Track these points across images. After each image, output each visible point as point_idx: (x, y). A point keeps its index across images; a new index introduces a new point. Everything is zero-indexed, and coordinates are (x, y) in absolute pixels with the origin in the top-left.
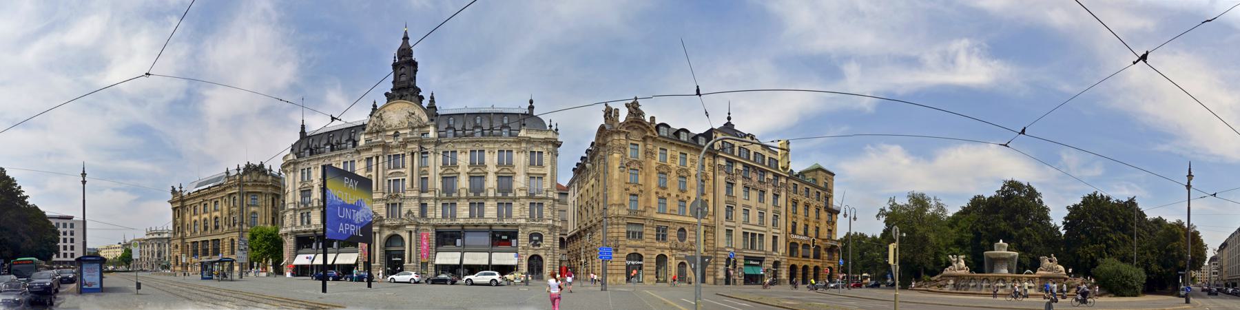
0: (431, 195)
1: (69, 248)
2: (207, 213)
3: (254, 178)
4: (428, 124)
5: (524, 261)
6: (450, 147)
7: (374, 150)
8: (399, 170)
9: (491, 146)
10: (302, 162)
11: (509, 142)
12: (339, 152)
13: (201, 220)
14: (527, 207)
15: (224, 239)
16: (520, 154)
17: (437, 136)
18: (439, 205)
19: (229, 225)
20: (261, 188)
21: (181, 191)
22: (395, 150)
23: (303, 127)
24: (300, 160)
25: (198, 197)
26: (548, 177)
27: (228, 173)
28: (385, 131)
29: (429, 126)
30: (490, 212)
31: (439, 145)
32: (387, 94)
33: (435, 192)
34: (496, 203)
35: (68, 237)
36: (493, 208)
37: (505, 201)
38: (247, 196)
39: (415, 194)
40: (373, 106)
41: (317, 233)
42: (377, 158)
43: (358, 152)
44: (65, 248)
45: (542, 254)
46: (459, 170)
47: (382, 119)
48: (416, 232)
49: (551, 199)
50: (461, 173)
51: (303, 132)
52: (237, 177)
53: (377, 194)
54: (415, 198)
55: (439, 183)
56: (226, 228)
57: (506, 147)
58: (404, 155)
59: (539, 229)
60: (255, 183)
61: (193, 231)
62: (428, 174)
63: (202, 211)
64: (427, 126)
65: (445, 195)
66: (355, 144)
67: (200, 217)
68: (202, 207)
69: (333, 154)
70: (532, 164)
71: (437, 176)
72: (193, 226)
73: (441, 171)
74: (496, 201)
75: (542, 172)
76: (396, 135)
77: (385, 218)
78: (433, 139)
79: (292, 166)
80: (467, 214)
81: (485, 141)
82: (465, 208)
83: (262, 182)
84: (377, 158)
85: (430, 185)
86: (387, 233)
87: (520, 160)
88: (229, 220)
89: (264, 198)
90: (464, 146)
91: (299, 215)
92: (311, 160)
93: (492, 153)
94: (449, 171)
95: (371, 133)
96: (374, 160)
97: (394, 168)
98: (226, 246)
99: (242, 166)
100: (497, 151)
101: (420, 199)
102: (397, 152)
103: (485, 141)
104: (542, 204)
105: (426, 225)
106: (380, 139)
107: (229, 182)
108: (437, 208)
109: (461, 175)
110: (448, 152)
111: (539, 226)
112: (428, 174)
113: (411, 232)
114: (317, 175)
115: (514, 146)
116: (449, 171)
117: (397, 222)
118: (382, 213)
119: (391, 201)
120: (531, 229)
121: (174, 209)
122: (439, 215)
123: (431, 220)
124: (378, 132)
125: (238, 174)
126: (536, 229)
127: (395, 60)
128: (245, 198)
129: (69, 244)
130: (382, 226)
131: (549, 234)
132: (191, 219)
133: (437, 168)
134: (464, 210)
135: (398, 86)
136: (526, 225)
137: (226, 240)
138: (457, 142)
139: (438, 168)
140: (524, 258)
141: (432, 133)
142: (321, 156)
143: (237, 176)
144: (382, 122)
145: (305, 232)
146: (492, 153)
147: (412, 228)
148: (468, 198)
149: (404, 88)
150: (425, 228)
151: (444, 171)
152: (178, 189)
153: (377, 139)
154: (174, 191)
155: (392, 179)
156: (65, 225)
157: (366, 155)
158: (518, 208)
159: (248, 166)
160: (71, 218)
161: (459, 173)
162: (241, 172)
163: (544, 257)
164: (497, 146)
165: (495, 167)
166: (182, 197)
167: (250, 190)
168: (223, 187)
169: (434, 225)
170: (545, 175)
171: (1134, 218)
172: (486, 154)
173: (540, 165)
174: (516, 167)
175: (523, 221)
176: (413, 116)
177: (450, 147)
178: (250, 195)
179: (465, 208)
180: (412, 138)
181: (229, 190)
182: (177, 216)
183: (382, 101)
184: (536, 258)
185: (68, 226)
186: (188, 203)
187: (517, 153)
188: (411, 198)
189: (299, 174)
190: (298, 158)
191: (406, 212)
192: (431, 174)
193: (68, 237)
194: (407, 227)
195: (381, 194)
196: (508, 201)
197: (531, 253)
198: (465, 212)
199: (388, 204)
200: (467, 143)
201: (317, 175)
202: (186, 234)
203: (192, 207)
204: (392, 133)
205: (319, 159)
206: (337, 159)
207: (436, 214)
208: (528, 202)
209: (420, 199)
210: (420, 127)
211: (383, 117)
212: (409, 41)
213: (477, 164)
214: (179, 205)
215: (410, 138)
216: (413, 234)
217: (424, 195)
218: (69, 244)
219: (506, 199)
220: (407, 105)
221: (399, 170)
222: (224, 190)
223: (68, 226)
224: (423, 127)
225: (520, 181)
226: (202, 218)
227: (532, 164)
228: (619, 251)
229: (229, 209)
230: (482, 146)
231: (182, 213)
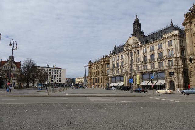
0: (140, 63)
1: (59, 79)
6: (144, 47)
14: (167, 62)
18: (142, 65)
23: (115, 46)
26: (174, 50)
28: (129, 46)
30: (157, 66)
32: (132, 34)
35: (59, 72)
37: (152, 63)
44: (58, 79)
45: (173, 80)
51: (115, 47)
52: (103, 59)
57: (169, 40)
59: (171, 70)
64: (138, 42)
65: (144, 63)
70: (169, 46)
75: (172, 48)
85: (140, 60)
87: (164, 46)
94: (145, 55)
99: (105, 56)
100: (157, 45)
104: (172, 60)
111: (172, 69)
115: (162, 41)
120: (169, 70)
122: (143, 69)
126: (170, 70)
129: (59, 77)
136: (166, 69)
156: (58, 71)
160: (60, 68)
163: (174, 81)
164: (157, 43)
166: (91, 64)
170: (173, 48)
171: (158, 79)
178: (107, 64)
184: (173, 82)
185: (59, 71)
186: (92, 66)
192: (140, 56)
193: (59, 72)
196: (162, 61)
200: (148, 45)
204: (131, 46)
207: (142, 68)
213: (152, 51)
217: (138, 63)
218: (59, 77)
223: (59, 71)
225: (165, 53)
227: (169, 46)
228: (192, 76)
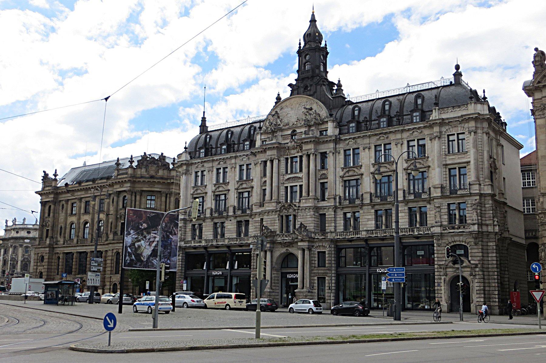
2: (89, 213)
3: (152, 173)
4: (326, 120)
5: (442, 284)
7: (269, 153)
8: (296, 175)
9: (399, 136)
10: (195, 163)
11: (419, 128)
12: (234, 155)
13: (79, 223)
14: (445, 210)
15: (106, 251)
16: (433, 140)
17: (337, 131)
19: (115, 233)
20: (160, 186)
21: (56, 180)
22: (293, 152)
23: (204, 120)
24: (194, 161)
25: (78, 190)
27: (118, 164)
29: (327, 122)
31: (339, 143)
33: (335, 199)
34: (406, 208)
38: (141, 195)
39: (310, 203)
40: (277, 99)
41: (209, 250)
42: (272, 161)
43: (254, 154)
46: (363, 170)
47: (279, 117)
48: (310, 250)
49: (476, 195)
50: (365, 174)
51: (203, 127)
53: (270, 205)
54: (310, 208)
55: (341, 187)
56: (111, 236)
58: (301, 157)
60: (152, 180)
61: (67, 235)
62: (327, 178)
63: (82, 211)
64: (324, 122)
66: (252, 143)
67: (79, 219)
68: (83, 205)
69: (228, 156)
71: (337, 179)
72: (68, 231)
73: (342, 173)
74: (406, 205)
76: (294, 133)
77: (278, 233)
78: (331, 137)
79: (184, 167)
80: (371, 225)
81: (390, 132)
82: (370, 217)
83: (162, 178)
84: (272, 161)
86: (280, 251)
88: (116, 227)
89: (163, 199)
90: (367, 141)
91: (189, 226)
92: (205, 162)
93: (399, 145)
94: (351, 173)
95: (266, 133)
96: (269, 164)
97: (292, 172)
98: (109, 262)
101: (316, 209)
102: (294, 153)
103: (390, 132)
105: (321, 241)
106: (274, 141)
107: (119, 177)
108: (338, 219)
109: (364, 176)
110: (350, 149)
111: (461, 234)
112: (327, 178)
113: (303, 250)
114: (211, 179)
116: (351, 173)
117: (288, 239)
118: (276, 227)
119: (284, 213)
121: (43, 204)
123: (329, 234)
124: (273, 132)
125: (131, 167)
126: (456, 238)
127: (300, 47)
128: (138, 198)
130: (273, 243)
131: (476, 244)
132: (66, 219)
133: (338, 169)
134: (369, 220)
135: (301, 76)
136: (442, 235)
137: (110, 253)
138: (359, 137)
139: (339, 170)
140: (442, 281)
141: (331, 129)
142: (215, 158)
143: (130, 170)
144: (279, 121)
145: (195, 248)
146: (399, 145)
147: (305, 244)
148: (372, 204)
149: (308, 78)
150: (321, 244)
151: (345, 174)
152: (51, 176)
153: (272, 140)
154: (46, 177)
155: (289, 185)
157: (262, 157)
158: (433, 212)
159: (144, 157)
161: (362, 174)
162: (135, 164)
164: (405, 135)
165: (404, 162)
167: (145, 189)
168: (110, 182)
169: (332, 241)
170: (468, 162)
172: (393, 146)
173: (461, 151)
174: (430, 159)
175: (437, 230)
176: (311, 112)
177: (352, 145)
179: (370, 217)
180: (308, 138)
181: (118, 186)
182: (46, 215)
183: (286, 94)
187: (431, 140)
188: (306, 208)
189: (342, 156)
190: (191, 158)
191: (299, 226)
192: (331, 177)
194: (299, 244)
195: (274, 204)
197: (451, 272)
198: (369, 222)
199: (282, 216)
200: (370, 136)
201: (211, 179)
202: (57, 241)
203: (70, 203)
204: (289, 132)
205: (213, 161)
206: (233, 161)
208: (445, 202)
209: (316, 209)
210: (316, 124)
211: (280, 115)
212: (317, 23)
214: (50, 198)
215: (304, 139)
216: (307, 252)
219: (418, 201)
220: (305, 100)
221: (296, 175)
222: (111, 185)
224: (321, 124)
226: (82, 221)
229: (117, 211)
230: (387, 138)
231: (54, 209)
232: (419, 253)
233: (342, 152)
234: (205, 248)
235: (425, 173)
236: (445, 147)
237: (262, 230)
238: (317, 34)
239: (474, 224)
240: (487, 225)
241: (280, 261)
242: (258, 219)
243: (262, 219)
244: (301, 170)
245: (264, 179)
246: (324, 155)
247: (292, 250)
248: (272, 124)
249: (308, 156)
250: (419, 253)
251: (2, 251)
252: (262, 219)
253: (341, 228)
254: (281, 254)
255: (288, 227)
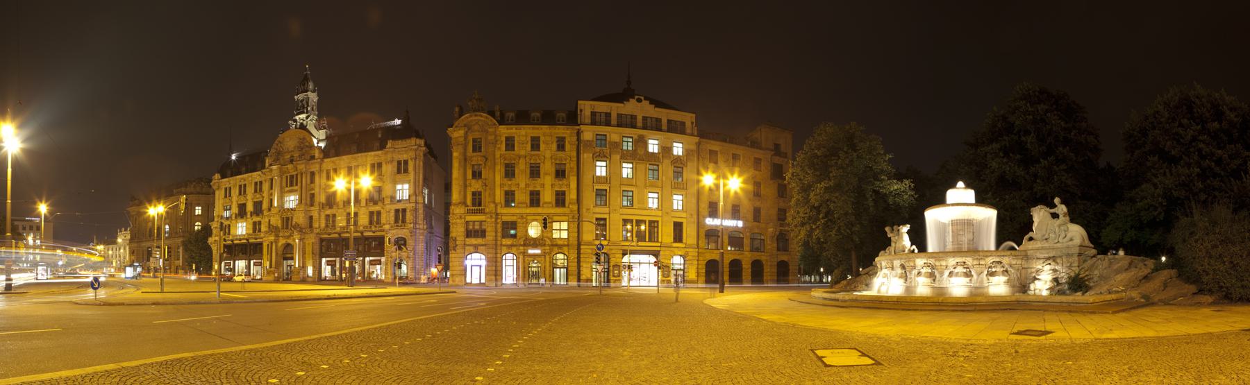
36: (365, 216)
58: (297, 175)
86: (282, 242)
189: (223, 190)
232: (478, 378)
233: (325, 171)
234: (232, 241)
235: (483, 223)
236: (395, 169)
237: (269, 227)
238: (822, 270)
239: (411, 223)
240: (419, 224)
241: (283, 247)
242: (267, 220)
243: (269, 221)
244: (297, 185)
245: (271, 192)
246: (313, 174)
247: (290, 241)
248: (816, 373)
249: (302, 174)
250: (478, 378)
251: (457, 109)
252: (269, 221)
253: (323, 225)
254: (282, 245)
255: (287, 225)
